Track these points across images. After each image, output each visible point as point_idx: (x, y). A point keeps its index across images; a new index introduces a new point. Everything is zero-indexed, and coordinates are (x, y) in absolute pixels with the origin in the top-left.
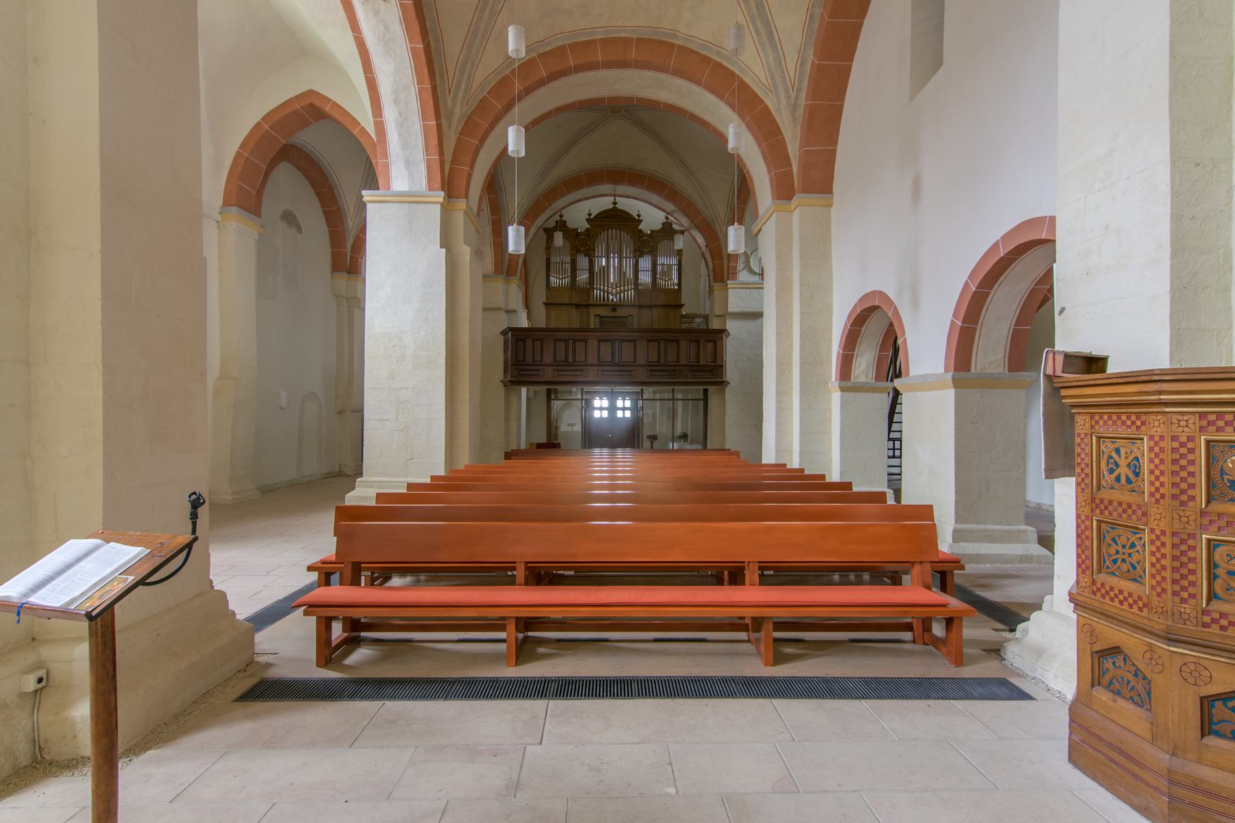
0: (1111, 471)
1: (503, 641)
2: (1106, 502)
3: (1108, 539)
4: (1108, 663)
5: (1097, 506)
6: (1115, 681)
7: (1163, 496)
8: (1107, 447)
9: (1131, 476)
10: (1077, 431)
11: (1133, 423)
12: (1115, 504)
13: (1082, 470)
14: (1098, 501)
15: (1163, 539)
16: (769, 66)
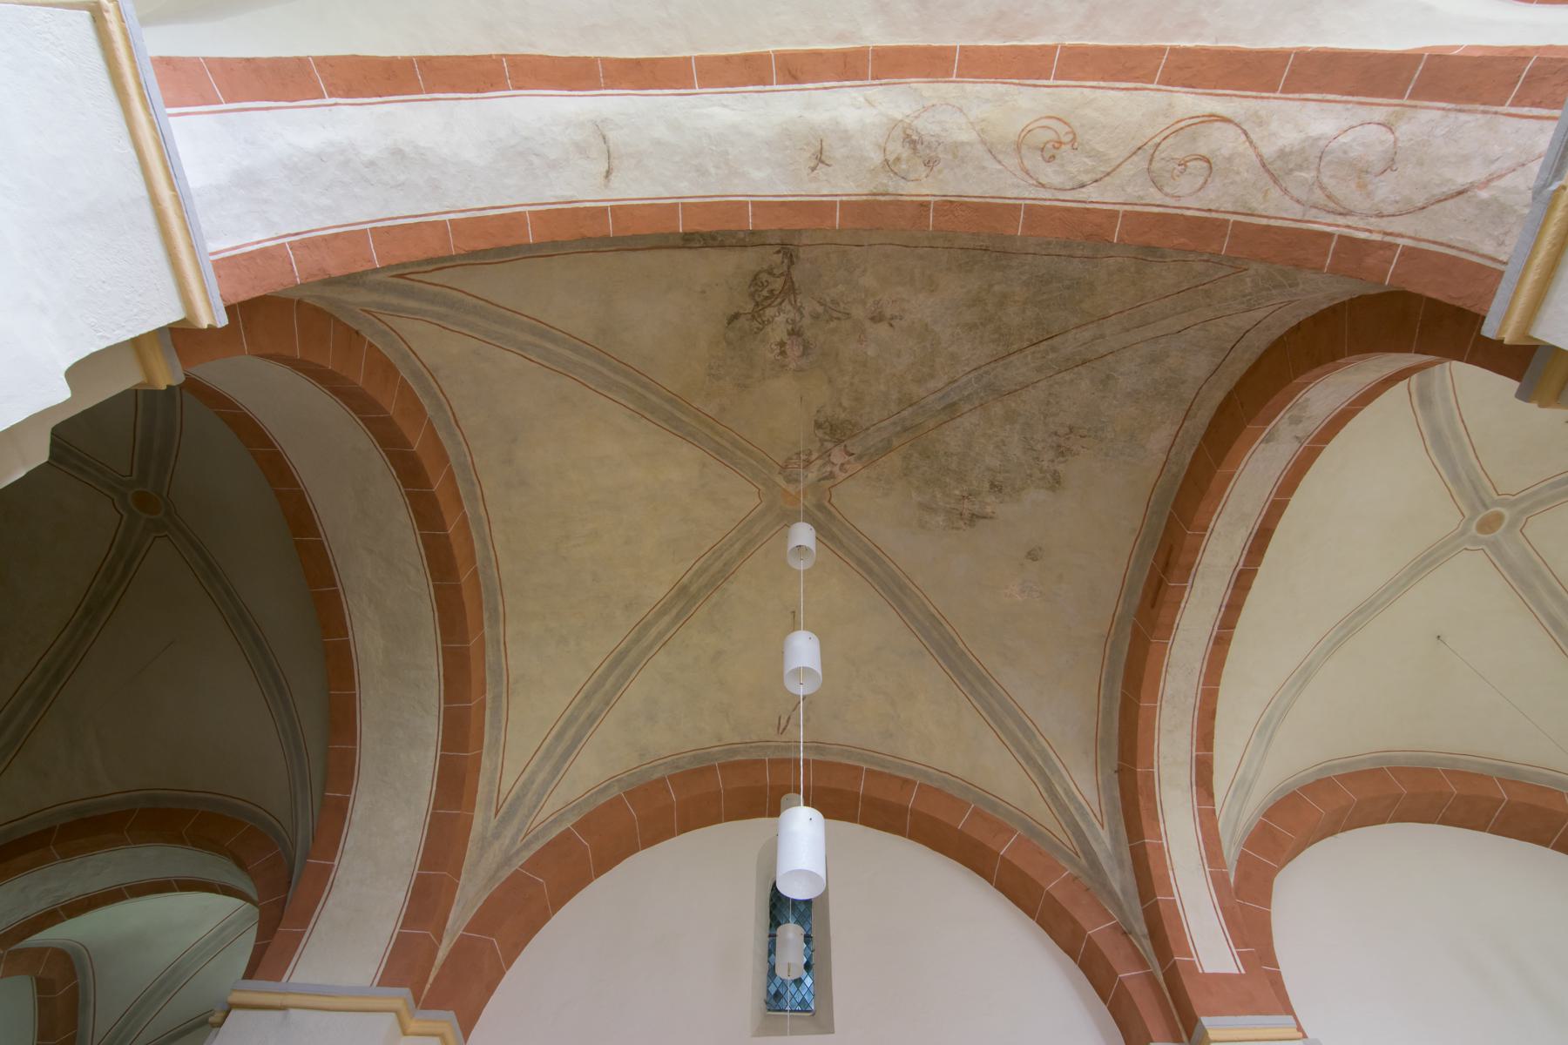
1: (1555, 118)
16: (531, 781)
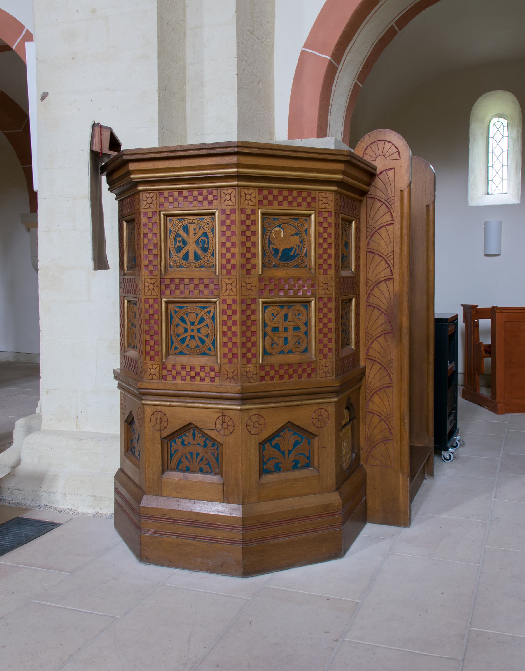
0: (179, 250)
2: (177, 282)
3: (176, 319)
4: (177, 444)
5: (167, 287)
6: (184, 459)
7: (234, 266)
8: (176, 224)
9: (200, 252)
10: (142, 210)
11: (205, 198)
12: (187, 281)
13: (150, 251)
14: (167, 282)
15: (234, 307)
